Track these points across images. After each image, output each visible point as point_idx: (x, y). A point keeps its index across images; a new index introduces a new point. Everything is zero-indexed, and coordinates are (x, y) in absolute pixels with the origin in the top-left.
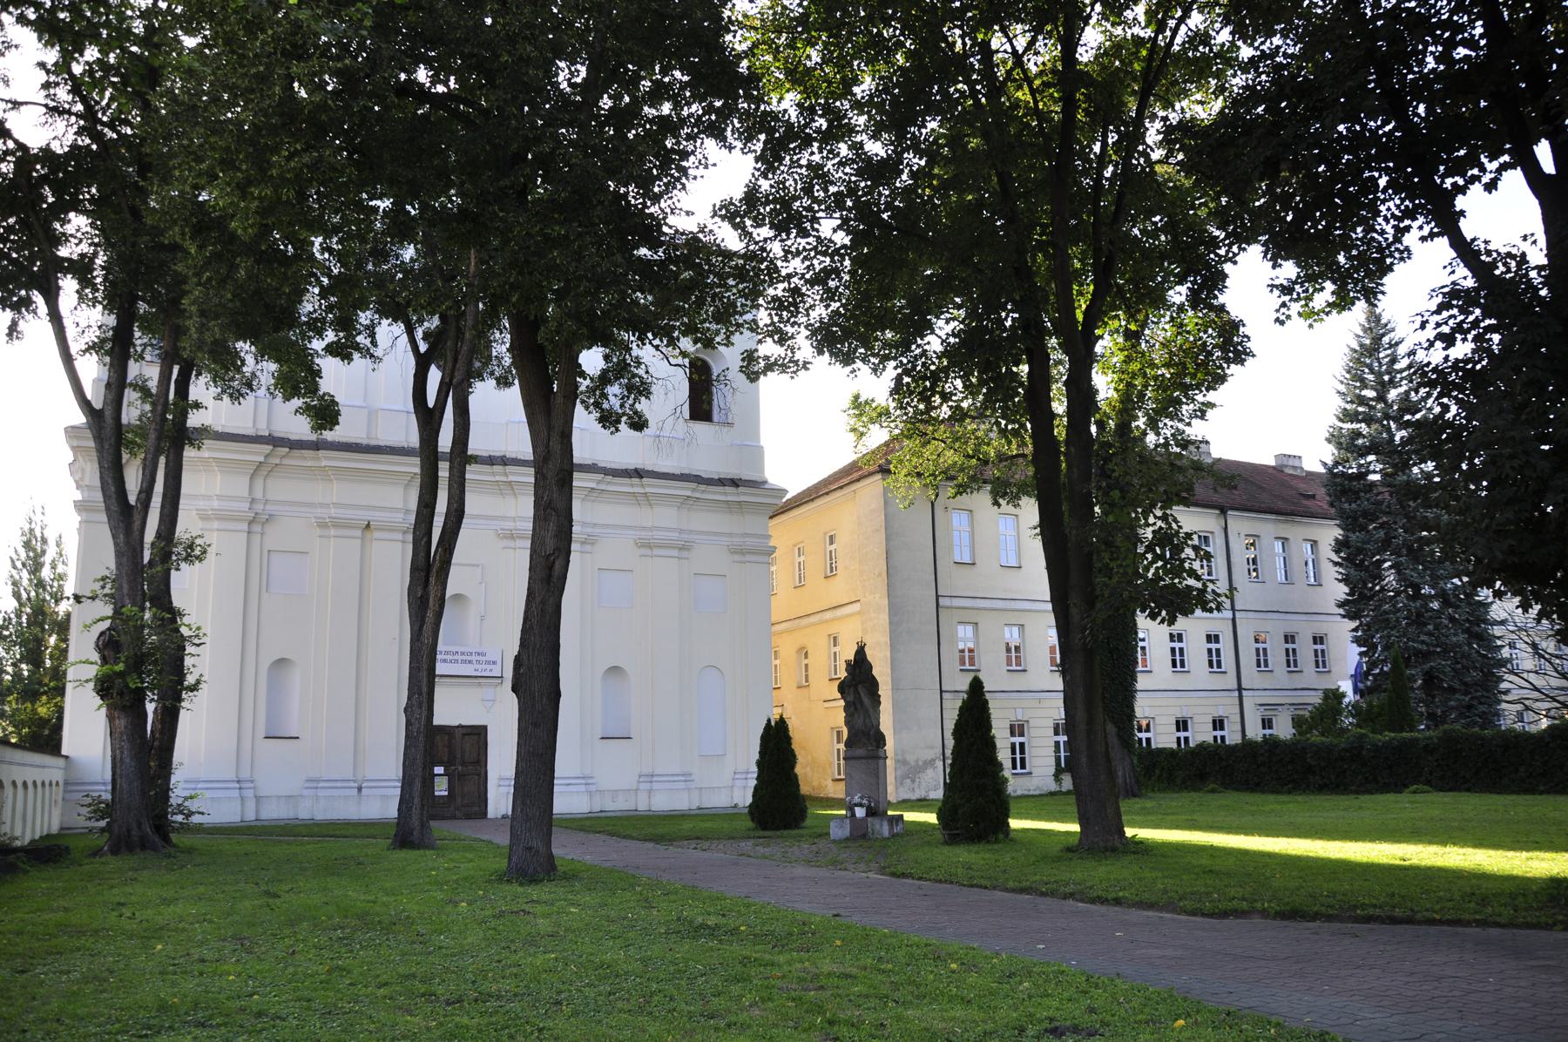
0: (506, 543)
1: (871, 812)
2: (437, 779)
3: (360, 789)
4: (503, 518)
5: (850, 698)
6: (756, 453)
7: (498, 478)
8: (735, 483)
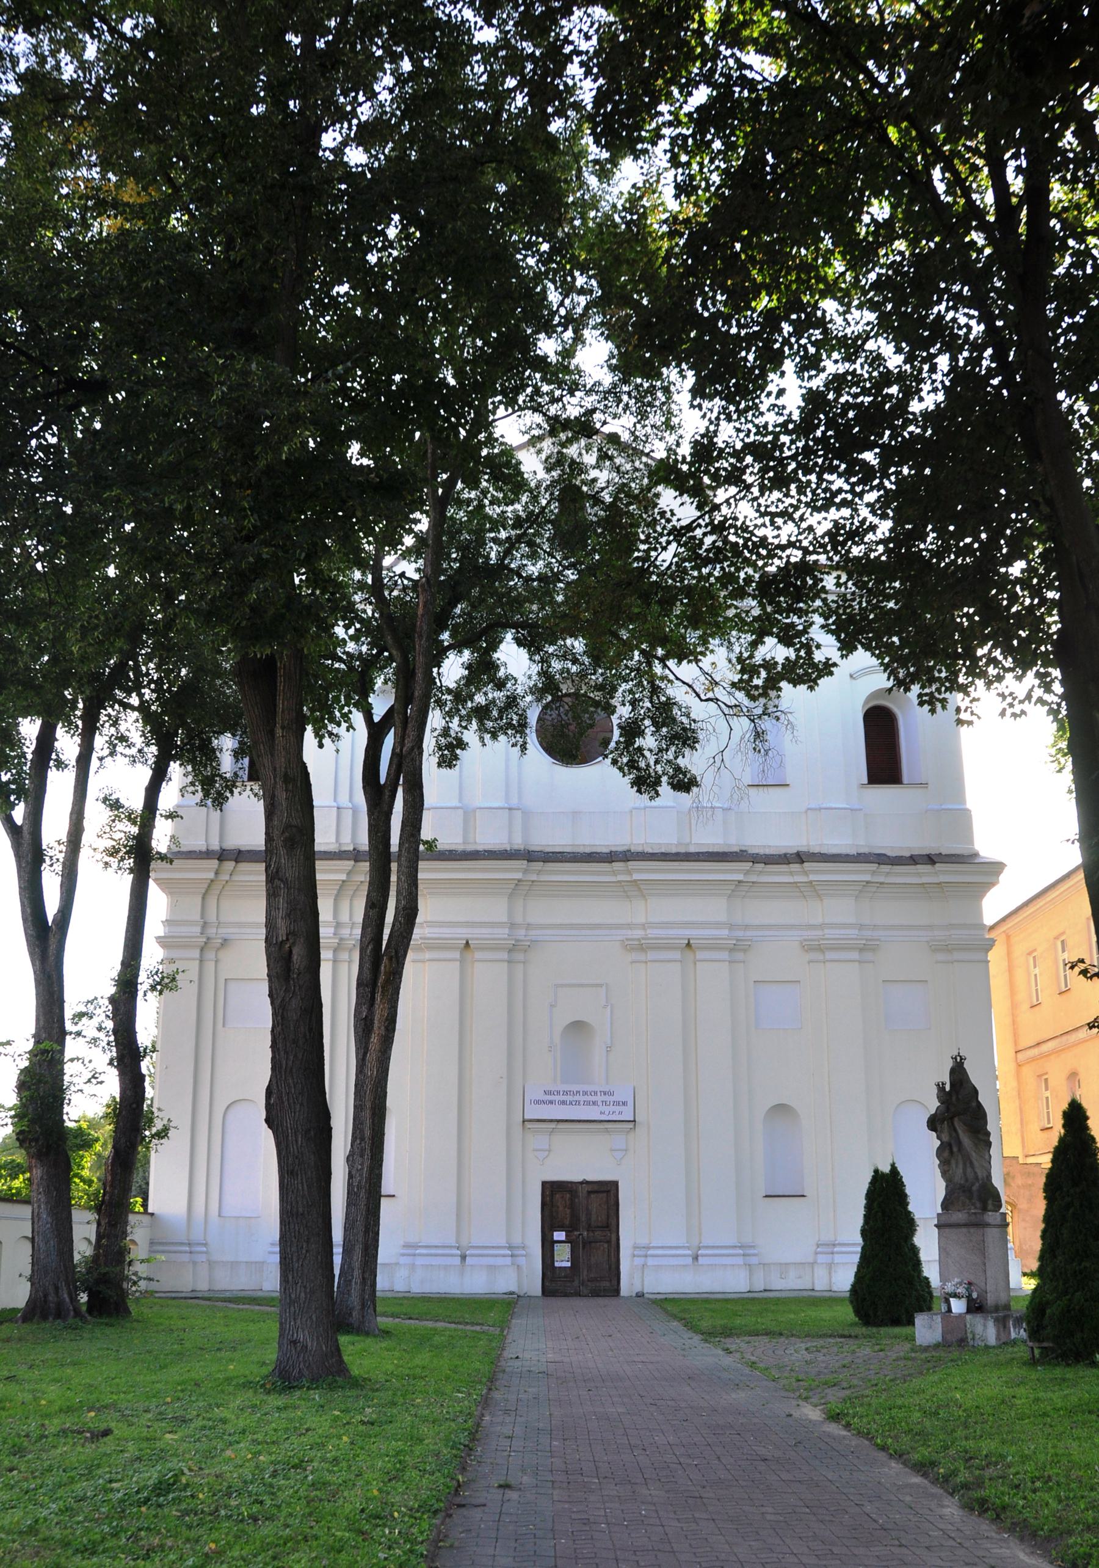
0: (634, 956)
1: (975, 1307)
2: (557, 1247)
3: (463, 1257)
4: (630, 926)
5: (946, 1138)
6: (962, 820)
7: (620, 878)
8: (931, 859)
